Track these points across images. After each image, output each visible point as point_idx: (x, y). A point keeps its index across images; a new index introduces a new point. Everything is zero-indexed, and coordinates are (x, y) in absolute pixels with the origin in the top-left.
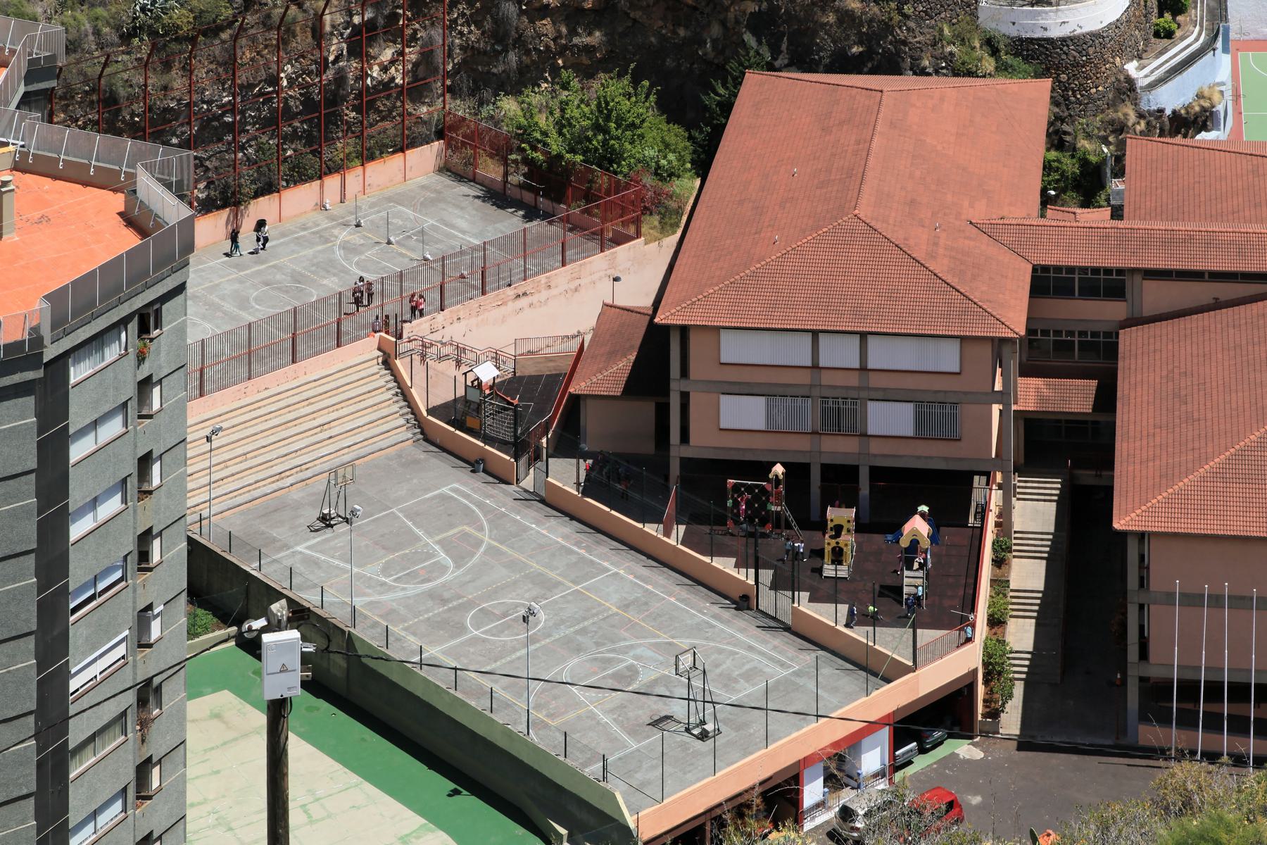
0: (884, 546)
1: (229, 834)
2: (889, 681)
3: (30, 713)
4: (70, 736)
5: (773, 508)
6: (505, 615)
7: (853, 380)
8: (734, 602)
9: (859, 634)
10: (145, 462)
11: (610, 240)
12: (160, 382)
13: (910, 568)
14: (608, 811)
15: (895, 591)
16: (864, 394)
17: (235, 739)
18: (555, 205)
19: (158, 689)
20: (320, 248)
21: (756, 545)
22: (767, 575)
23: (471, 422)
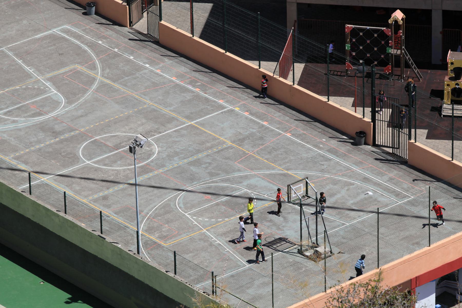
5: (393, 51)
8: (351, 138)
22: (385, 114)
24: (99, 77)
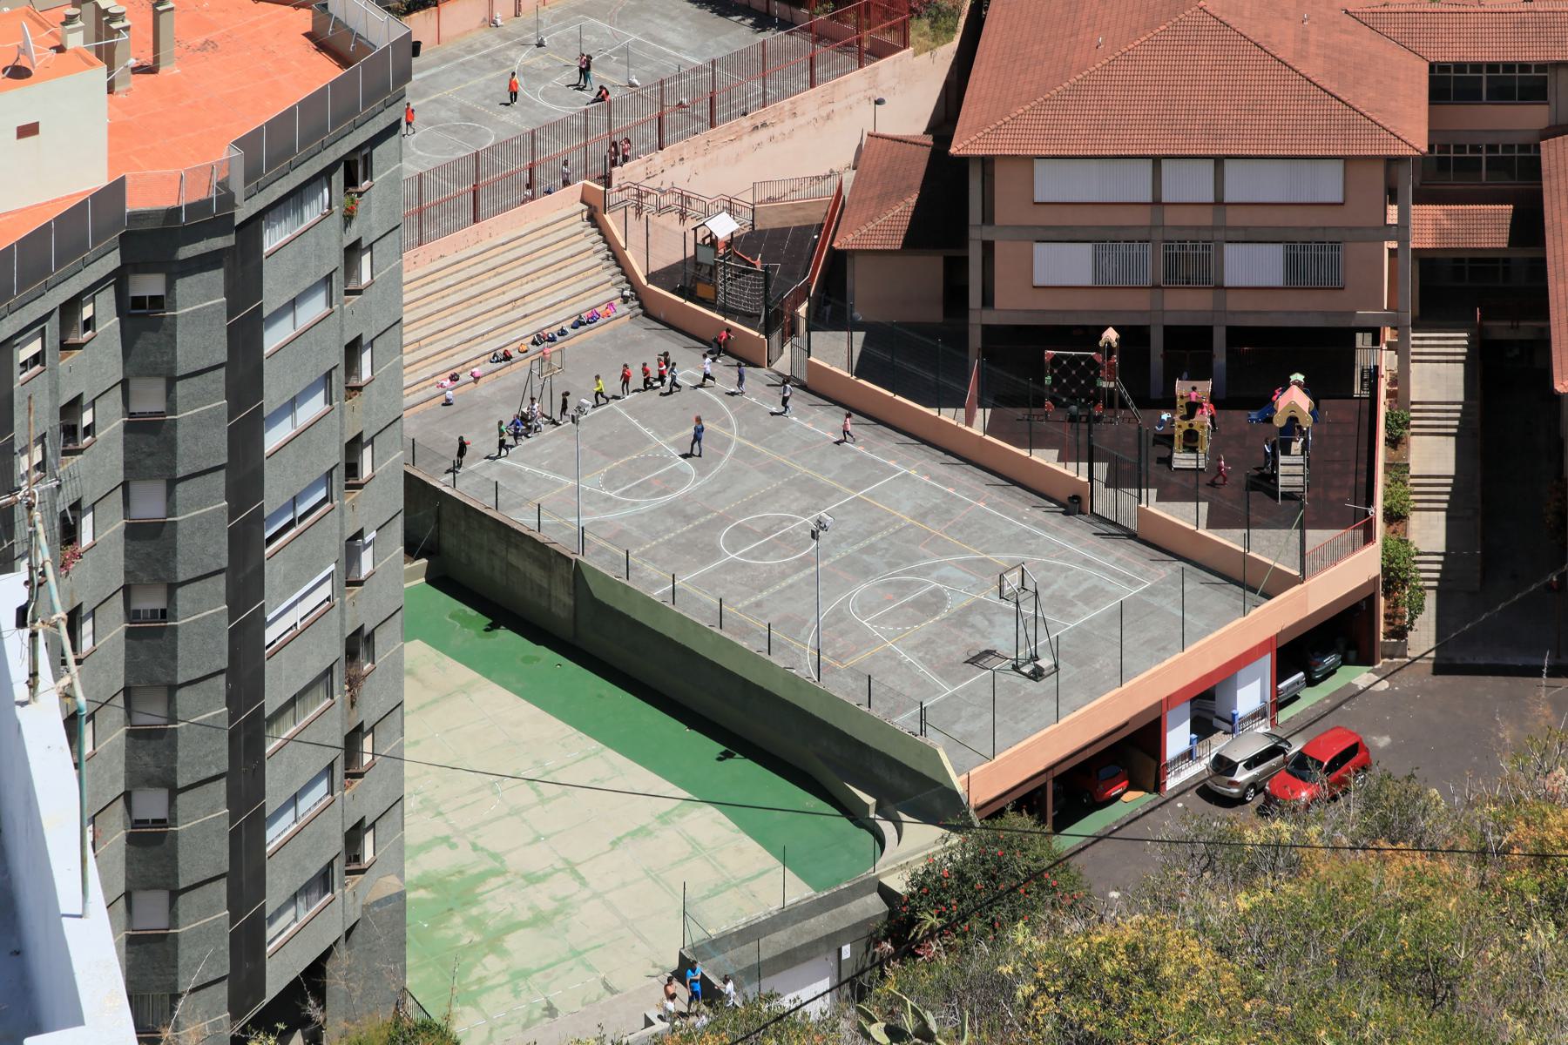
0: (1247, 428)
1: (438, 820)
2: (1269, 597)
3: (221, 672)
4: (266, 700)
5: (1104, 385)
6: (767, 533)
7: (1206, 218)
8: (1061, 505)
9: (1230, 539)
10: (353, 350)
11: (869, 52)
12: (370, 247)
13: (1287, 452)
14: (927, 772)
15: (1264, 481)
16: (1218, 235)
17: (435, 701)
18: (794, 10)
19: (370, 638)
20: (493, 75)
21: (1090, 430)
22: (1101, 469)
23: (703, 290)
24: (735, 437)
